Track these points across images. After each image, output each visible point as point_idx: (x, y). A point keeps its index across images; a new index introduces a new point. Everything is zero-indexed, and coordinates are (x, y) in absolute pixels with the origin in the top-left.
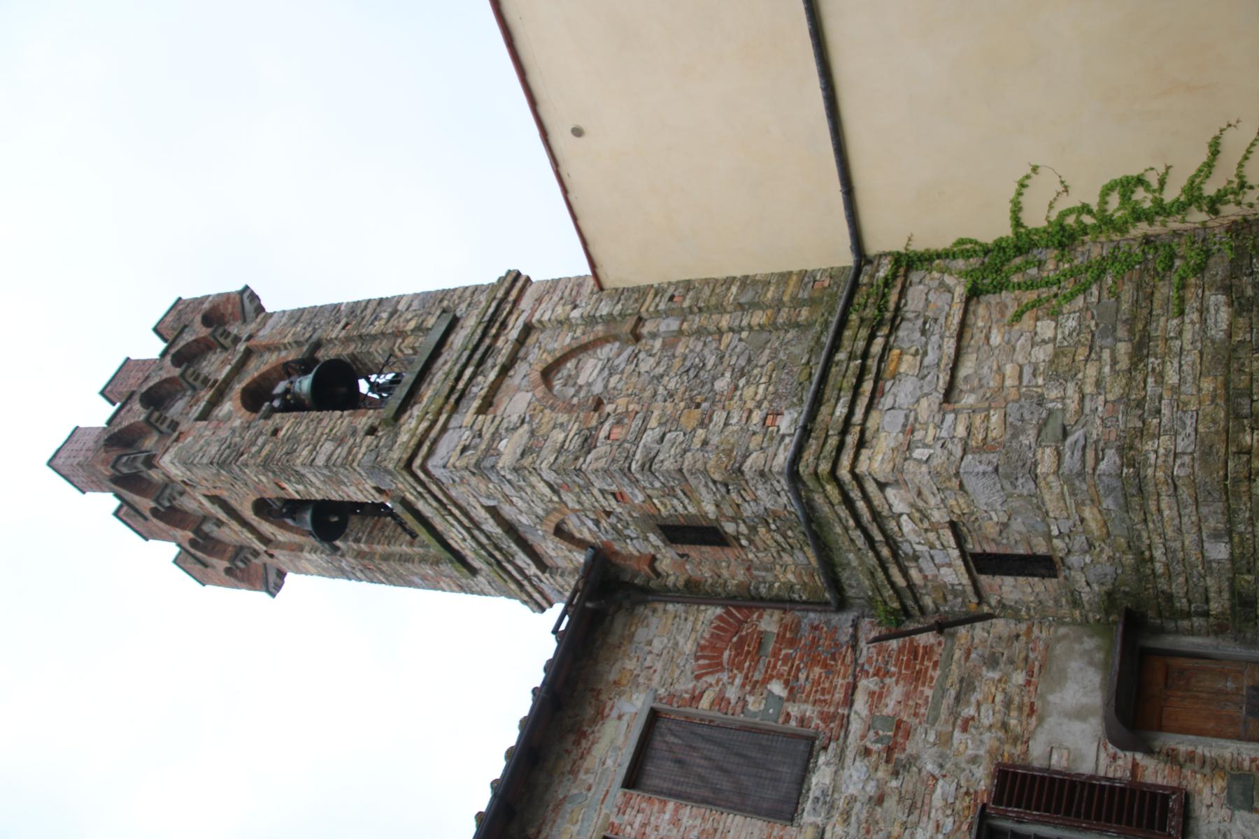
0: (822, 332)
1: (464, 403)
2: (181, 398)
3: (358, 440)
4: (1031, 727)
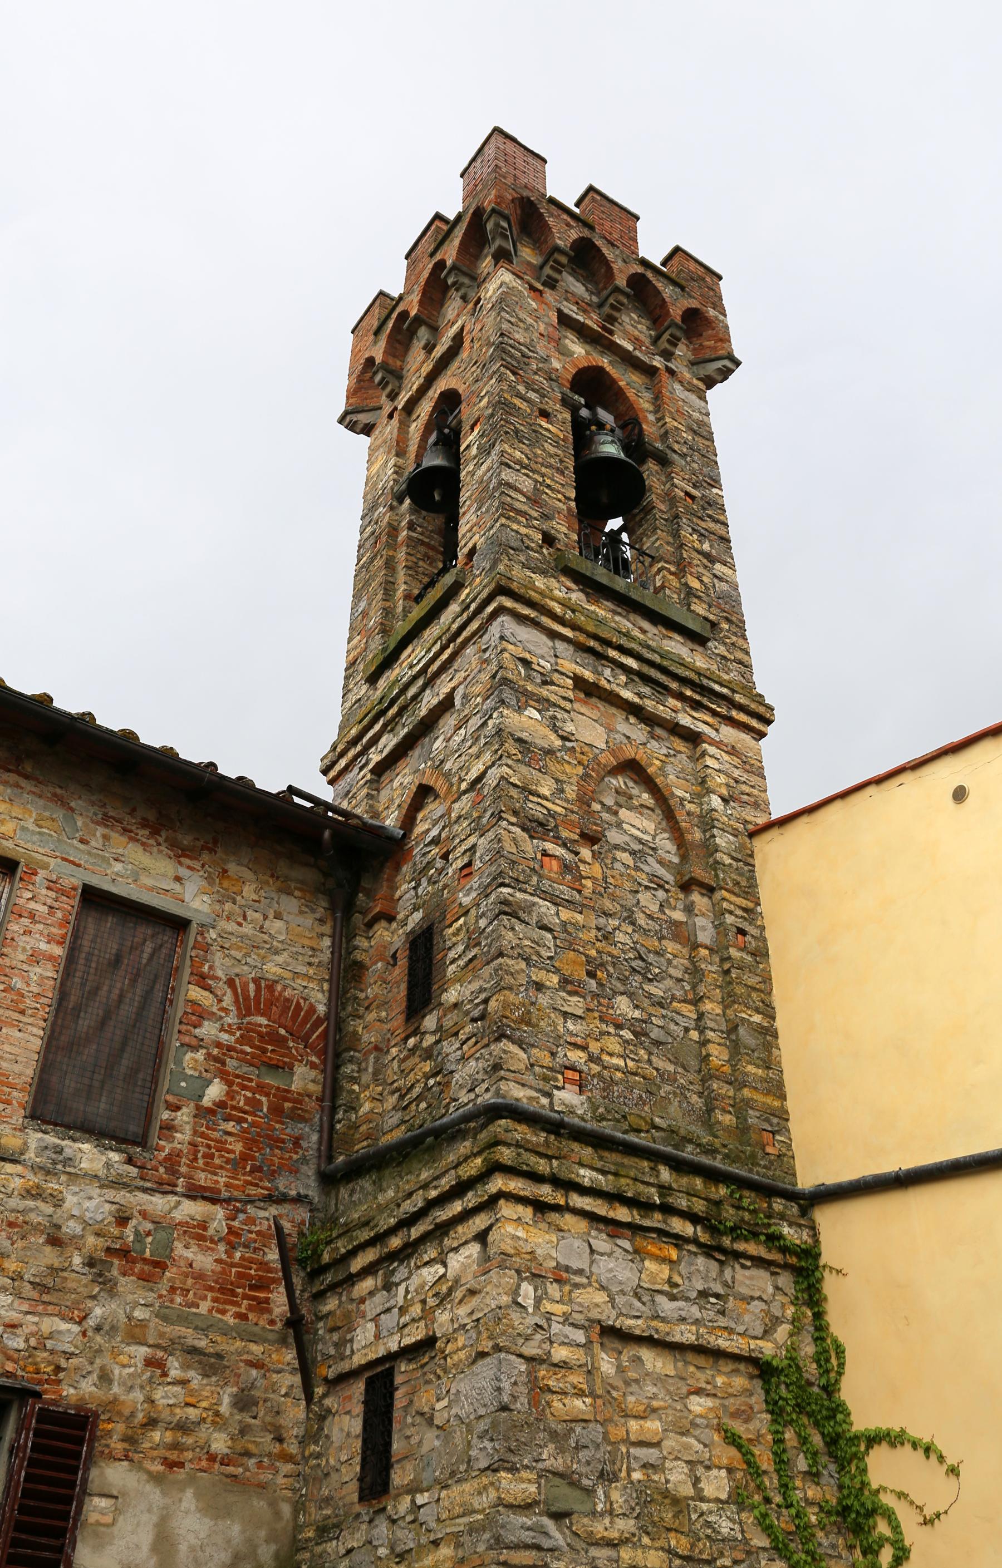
0: (699, 1145)
1: (590, 659)
2: (587, 290)
3: (535, 522)
4: (148, 1465)
